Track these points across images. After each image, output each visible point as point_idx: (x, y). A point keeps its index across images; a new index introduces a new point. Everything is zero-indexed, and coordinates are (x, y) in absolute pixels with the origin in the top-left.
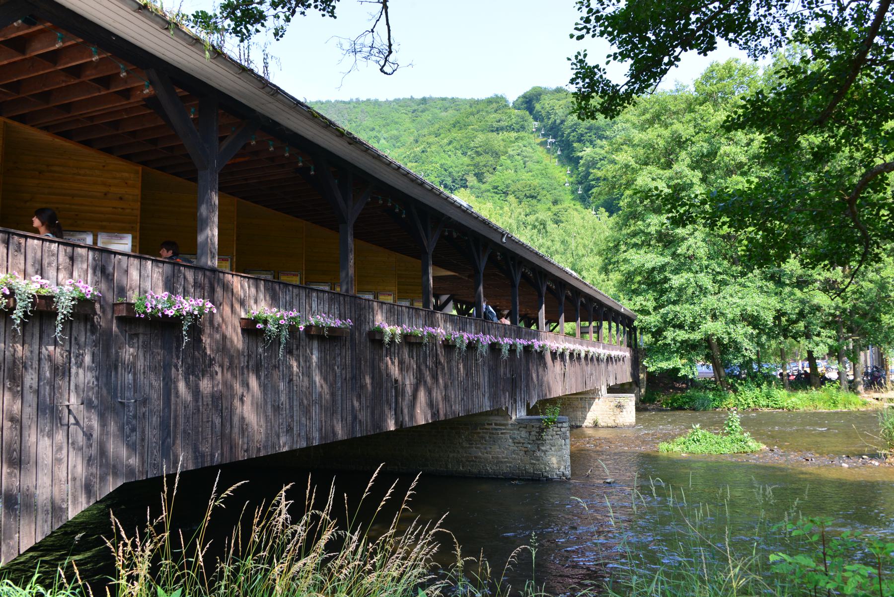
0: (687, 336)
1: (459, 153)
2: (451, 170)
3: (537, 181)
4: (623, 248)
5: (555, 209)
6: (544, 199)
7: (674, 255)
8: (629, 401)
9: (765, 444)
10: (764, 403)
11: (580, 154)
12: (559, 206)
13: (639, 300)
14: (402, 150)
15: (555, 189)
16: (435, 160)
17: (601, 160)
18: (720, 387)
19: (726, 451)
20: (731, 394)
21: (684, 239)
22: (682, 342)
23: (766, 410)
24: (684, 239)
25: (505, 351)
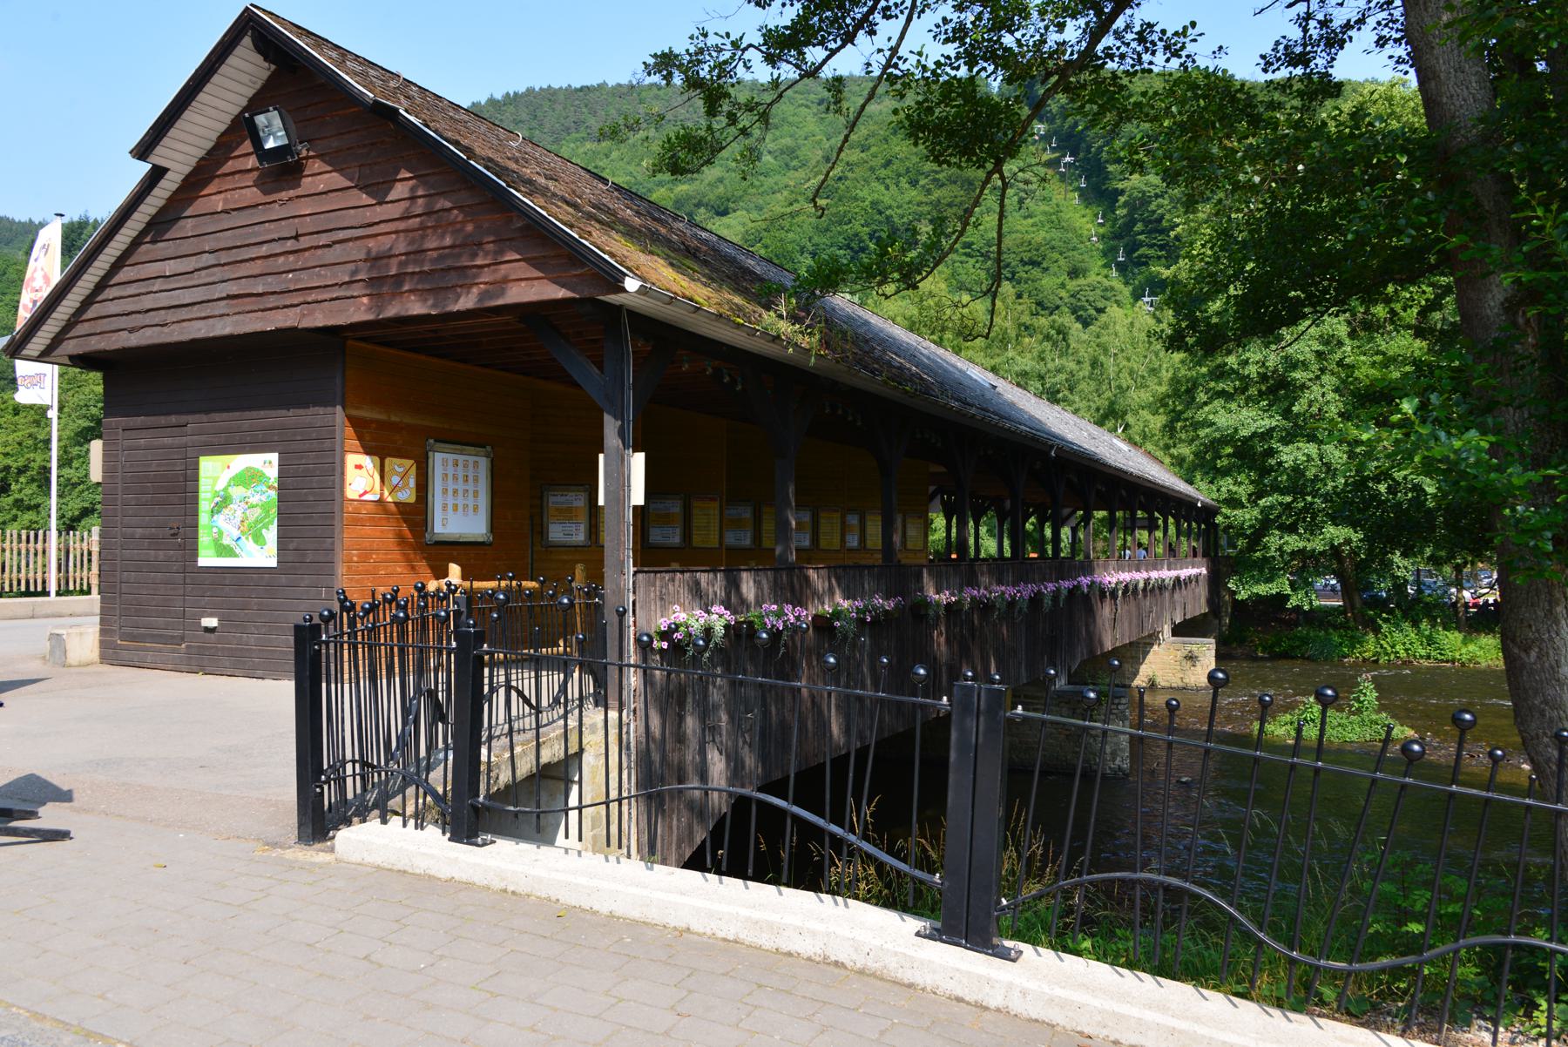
0: (1301, 545)
1: (903, 181)
2: (888, 212)
3: (1042, 234)
4: (1202, 397)
5: (1072, 285)
6: (1054, 268)
7: (1287, 414)
8: (1206, 651)
9: (1412, 727)
10: (1423, 653)
11: (1120, 186)
12: (1081, 281)
13: (1227, 484)
14: (801, 174)
15: (1074, 249)
16: (861, 194)
17: (1157, 196)
18: (1352, 624)
19: (1355, 738)
20: (1371, 637)
21: (1303, 387)
22: (1293, 553)
23: (1425, 663)
24: (1303, 387)
25: (1048, 602)
